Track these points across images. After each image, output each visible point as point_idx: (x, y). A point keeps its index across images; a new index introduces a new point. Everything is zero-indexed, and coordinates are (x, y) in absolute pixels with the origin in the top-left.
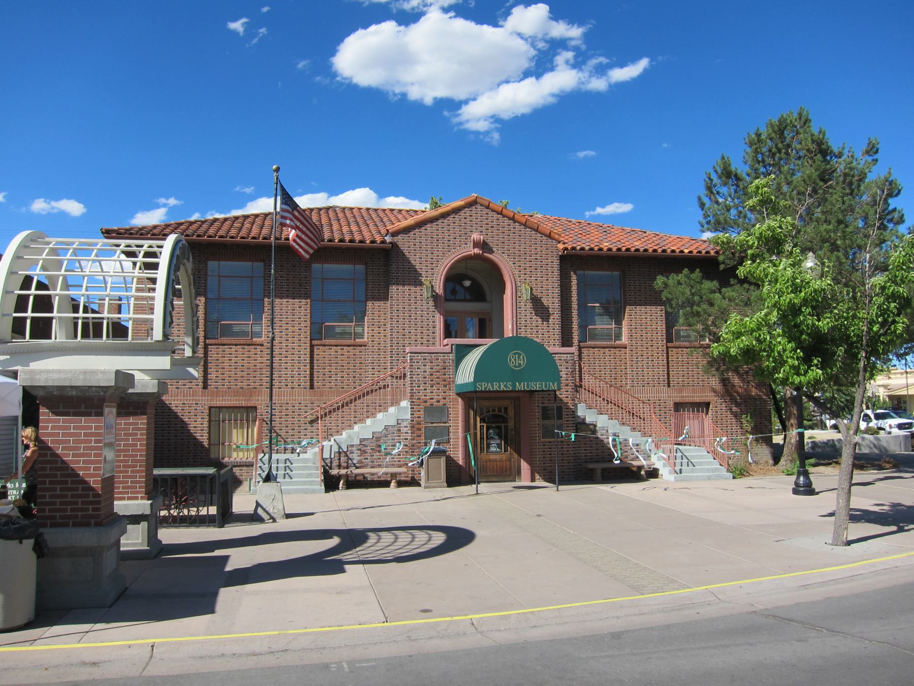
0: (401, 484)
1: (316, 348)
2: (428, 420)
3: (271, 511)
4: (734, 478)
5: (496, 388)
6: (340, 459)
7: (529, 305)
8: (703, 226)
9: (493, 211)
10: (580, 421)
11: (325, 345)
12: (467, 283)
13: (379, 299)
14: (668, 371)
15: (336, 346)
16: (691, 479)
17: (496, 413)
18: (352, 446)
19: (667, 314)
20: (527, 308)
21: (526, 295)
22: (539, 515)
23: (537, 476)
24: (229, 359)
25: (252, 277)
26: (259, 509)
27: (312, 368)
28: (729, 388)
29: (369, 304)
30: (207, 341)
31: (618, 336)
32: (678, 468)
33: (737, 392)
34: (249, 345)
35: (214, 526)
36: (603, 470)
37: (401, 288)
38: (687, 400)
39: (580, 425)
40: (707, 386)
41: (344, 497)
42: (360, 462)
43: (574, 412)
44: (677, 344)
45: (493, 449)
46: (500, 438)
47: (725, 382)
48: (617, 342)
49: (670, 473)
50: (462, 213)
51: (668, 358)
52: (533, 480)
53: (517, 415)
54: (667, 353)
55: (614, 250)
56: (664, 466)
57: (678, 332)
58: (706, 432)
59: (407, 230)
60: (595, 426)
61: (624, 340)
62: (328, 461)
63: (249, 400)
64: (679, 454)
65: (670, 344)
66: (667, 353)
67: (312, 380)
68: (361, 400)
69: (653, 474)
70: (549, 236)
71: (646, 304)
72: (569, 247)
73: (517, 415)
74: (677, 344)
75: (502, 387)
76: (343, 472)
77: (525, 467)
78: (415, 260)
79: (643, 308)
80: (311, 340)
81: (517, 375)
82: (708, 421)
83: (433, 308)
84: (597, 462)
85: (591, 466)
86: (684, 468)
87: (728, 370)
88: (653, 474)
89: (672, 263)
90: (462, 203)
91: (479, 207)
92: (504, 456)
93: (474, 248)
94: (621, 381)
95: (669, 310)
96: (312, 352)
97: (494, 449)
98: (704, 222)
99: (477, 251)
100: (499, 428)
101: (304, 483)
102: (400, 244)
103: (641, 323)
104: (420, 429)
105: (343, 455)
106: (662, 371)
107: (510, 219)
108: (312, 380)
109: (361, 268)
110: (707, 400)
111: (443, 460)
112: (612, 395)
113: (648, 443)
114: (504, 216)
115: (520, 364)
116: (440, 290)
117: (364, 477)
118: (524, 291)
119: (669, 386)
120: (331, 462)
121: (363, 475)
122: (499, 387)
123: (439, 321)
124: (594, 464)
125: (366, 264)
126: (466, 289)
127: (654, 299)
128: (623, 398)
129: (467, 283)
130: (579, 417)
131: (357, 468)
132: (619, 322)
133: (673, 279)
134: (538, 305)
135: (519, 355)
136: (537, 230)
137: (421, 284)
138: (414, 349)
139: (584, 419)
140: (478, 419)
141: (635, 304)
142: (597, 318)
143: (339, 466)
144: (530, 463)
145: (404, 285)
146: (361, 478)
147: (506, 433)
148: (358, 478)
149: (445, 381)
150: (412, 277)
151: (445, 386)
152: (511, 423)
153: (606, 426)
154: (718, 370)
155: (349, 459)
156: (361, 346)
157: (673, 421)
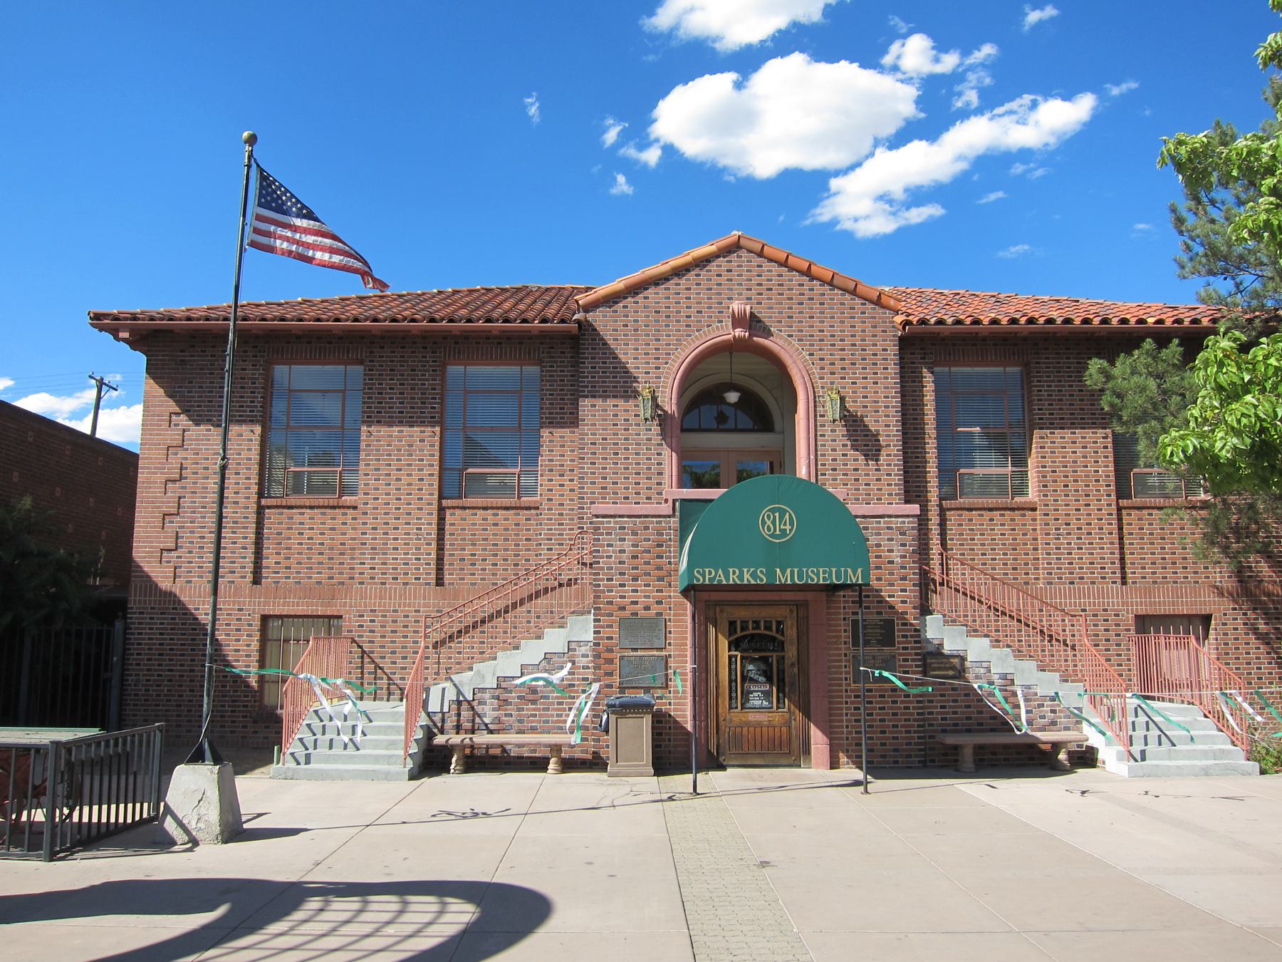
0: (569, 765)
1: (448, 512)
2: (627, 644)
3: (192, 826)
4: (1263, 772)
5: (733, 579)
6: (459, 715)
7: (841, 430)
8: (1183, 267)
9: (771, 260)
10: (931, 648)
11: (464, 508)
12: (733, 397)
13: (562, 425)
14: (1122, 553)
15: (485, 508)
16: (1165, 773)
17: (762, 631)
18: (483, 690)
19: (1117, 440)
20: (836, 435)
21: (832, 410)
22: (764, 864)
23: (843, 759)
24: (301, 531)
25: (343, 391)
26: (169, 818)
27: (440, 548)
28: (1252, 585)
29: (545, 433)
30: (263, 502)
31: (1021, 489)
32: (1136, 749)
33: (1268, 595)
34: (334, 507)
35: (39, 858)
36: (979, 749)
37: (599, 402)
38: (1161, 610)
39: (932, 660)
40: (1203, 583)
41: (457, 788)
42: (498, 720)
43: (918, 633)
44: (1136, 501)
45: (756, 701)
46: (769, 680)
47: (1242, 575)
48: (1017, 499)
49: (1120, 759)
50: (713, 266)
51: (1120, 529)
52: (834, 765)
53: (802, 637)
54: (1120, 519)
55: (1004, 321)
56: (1108, 743)
57: (1141, 478)
58: (1205, 674)
59: (611, 300)
60: (963, 659)
61: (1032, 494)
62: (437, 718)
63: (329, 605)
64: (1142, 719)
65: (1123, 503)
66: (1120, 519)
67: (440, 569)
68: (524, 608)
69: (1086, 758)
70: (878, 302)
71: (1073, 426)
72: (915, 321)
73: (802, 637)
74: (1136, 501)
75: (747, 578)
76: (456, 739)
77: (818, 739)
78: (628, 354)
79: (1067, 434)
80: (441, 497)
81: (777, 554)
82: (1208, 652)
83: (657, 439)
84: (992, 730)
85: (951, 740)
86: (1152, 747)
87: (1246, 550)
88: (1086, 758)
89: (1115, 340)
90: (713, 248)
91: (743, 253)
92: (777, 717)
93: (734, 328)
94: (1028, 575)
95: (1119, 429)
96: (441, 519)
97: (757, 703)
98: (1184, 258)
99: (739, 332)
100: (764, 660)
101: (376, 759)
102: (599, 326)
103: (1066, 461)
104: (611, 661)
105: (465, 706)
106: (1109, 552)
107: (801, 273)
108: (440, 569)
109: (533, 370)
110: (1205, 610)
111: (647, 721)
112: (1012, 602)
113: (1072, 695)
114: (792, 269)
115: (783, 531)
116: (670, 404)
117: (504, 750)
118: (828, 404)
119: (1124, 583)
120: (443, 721)
121: (501, 746)
122: (741, 577)
123: (669, 462)
124: (968, 740)
125: (540, 362)
126: (735, 405)
127: (1086, 412)
128: (1031, 611)
129: (733, 397)
130: (928, 641)
131: (491, 732)
132: (1020, 461)
133: (1122, 366)
134: (855, 427)
135: (783, 513)
136: (854, 292)
137: (636, 394)
138: (600, 508)
139: (941, 645)
140: (724, 643)
141: (1052, 426)
142: (978, 457)
143: (458, 729)
144: (829, 732)
145: (605, 397)
146: (498, 751)
147: (781, 672)
148: (491, 751)
149: (659, 568)
150: (621, 384)
151: (661, 579)
152: (791, 652)
153: (986, 659)
154: (1225, 549)
155: (476, 714)
156: (529, 508)
157: (1133, 650)
